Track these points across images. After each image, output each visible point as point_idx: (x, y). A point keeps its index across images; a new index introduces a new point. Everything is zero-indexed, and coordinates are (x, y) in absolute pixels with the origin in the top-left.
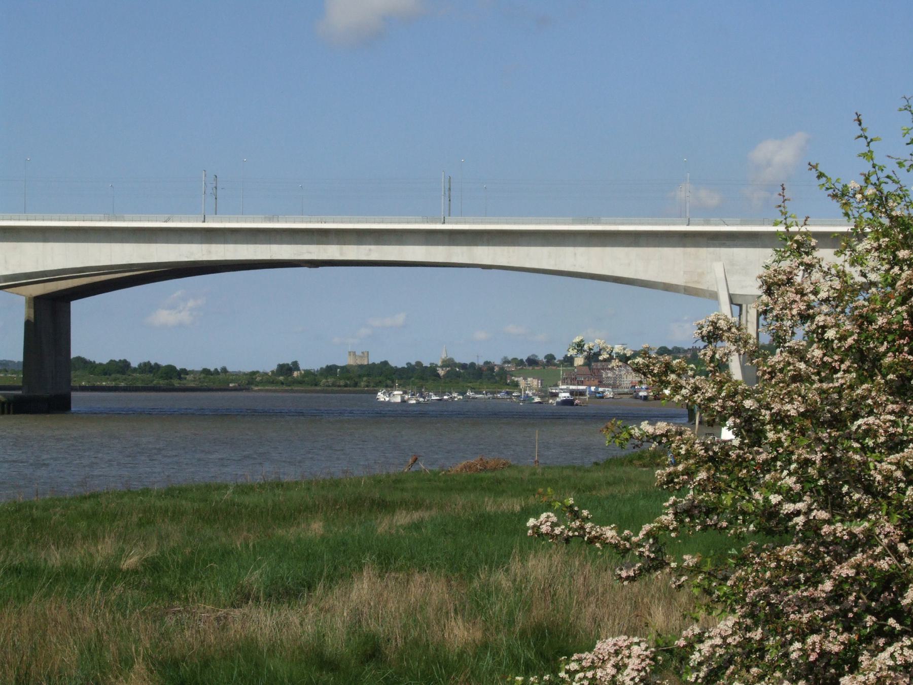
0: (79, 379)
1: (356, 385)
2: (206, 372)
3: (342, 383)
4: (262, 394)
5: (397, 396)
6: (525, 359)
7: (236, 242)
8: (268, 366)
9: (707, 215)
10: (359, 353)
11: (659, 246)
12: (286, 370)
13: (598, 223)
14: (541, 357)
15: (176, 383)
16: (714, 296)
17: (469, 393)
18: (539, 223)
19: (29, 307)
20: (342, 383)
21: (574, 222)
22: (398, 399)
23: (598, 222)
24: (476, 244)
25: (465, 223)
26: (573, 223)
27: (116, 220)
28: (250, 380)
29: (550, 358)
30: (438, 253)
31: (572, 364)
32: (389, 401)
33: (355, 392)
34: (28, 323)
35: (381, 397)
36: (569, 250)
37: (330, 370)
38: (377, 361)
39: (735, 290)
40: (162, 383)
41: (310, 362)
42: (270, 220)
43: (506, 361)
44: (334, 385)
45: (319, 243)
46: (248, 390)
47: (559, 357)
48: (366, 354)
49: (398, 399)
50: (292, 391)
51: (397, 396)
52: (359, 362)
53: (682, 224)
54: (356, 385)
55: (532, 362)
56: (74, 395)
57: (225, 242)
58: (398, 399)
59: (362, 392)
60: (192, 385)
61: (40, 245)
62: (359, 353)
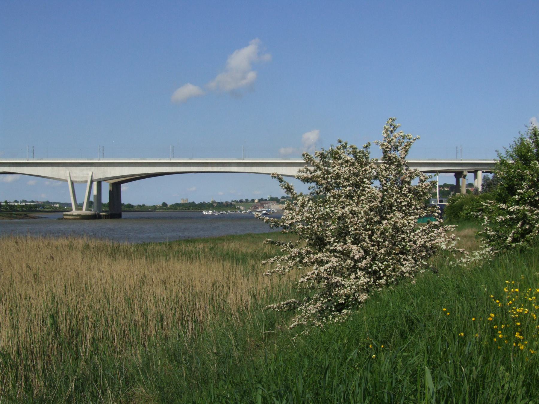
0: (122, 207)
1: (189, 209)
2: (139, 206)
3: (184, 209)
4: (159, 213)
5: (210, 212)
6: (239, 200)
7: (180, 166)
8: (160, 204)
9: (285, 157)
10: (185, 199)
11: (141, 166)
12: (165, 204)
13: (290, 160)
14: (244, 200)
15: (132, 209)
16: (66, 181)
17: (229, 212)
18: (110, 160)
19: (110, 186)
20: (184, 209)
21: (282, 160)
22: (211, 214)
23: (290, 160)
24: (252, 166)
25: (250, 160)
26: (282, 160)
27: (144, 160)
28: (154, 208)
29: (247, 200)
30: (215, 169)
31: (254, 202)
32: (207, 215)
33: (189, 212)
34: (110, 191)
35: (204, 213)
36: (284, 168)
37: (177, 205)
38: (191, 202)
39: (73, 179)
40: (128, 209)
41: (170, 202)
42: (191, 160)
43: (233, 201)
44: (182, 209)
45: (205, 166)
46: (155, 211)
47: (250, 199)
48: (187, 199)
49: (211, 214)
50: (168, 211)
51: (210, 212)
52: (185, 202)
53: (168, 160)
54: (189, 209)
55: (241, 201)
56: (122, 213)
57: (177, 166)
58: (211, 214)
59: (191, 212)
60: (137, 210)
61: (121, 168)
62: (185, 199)
